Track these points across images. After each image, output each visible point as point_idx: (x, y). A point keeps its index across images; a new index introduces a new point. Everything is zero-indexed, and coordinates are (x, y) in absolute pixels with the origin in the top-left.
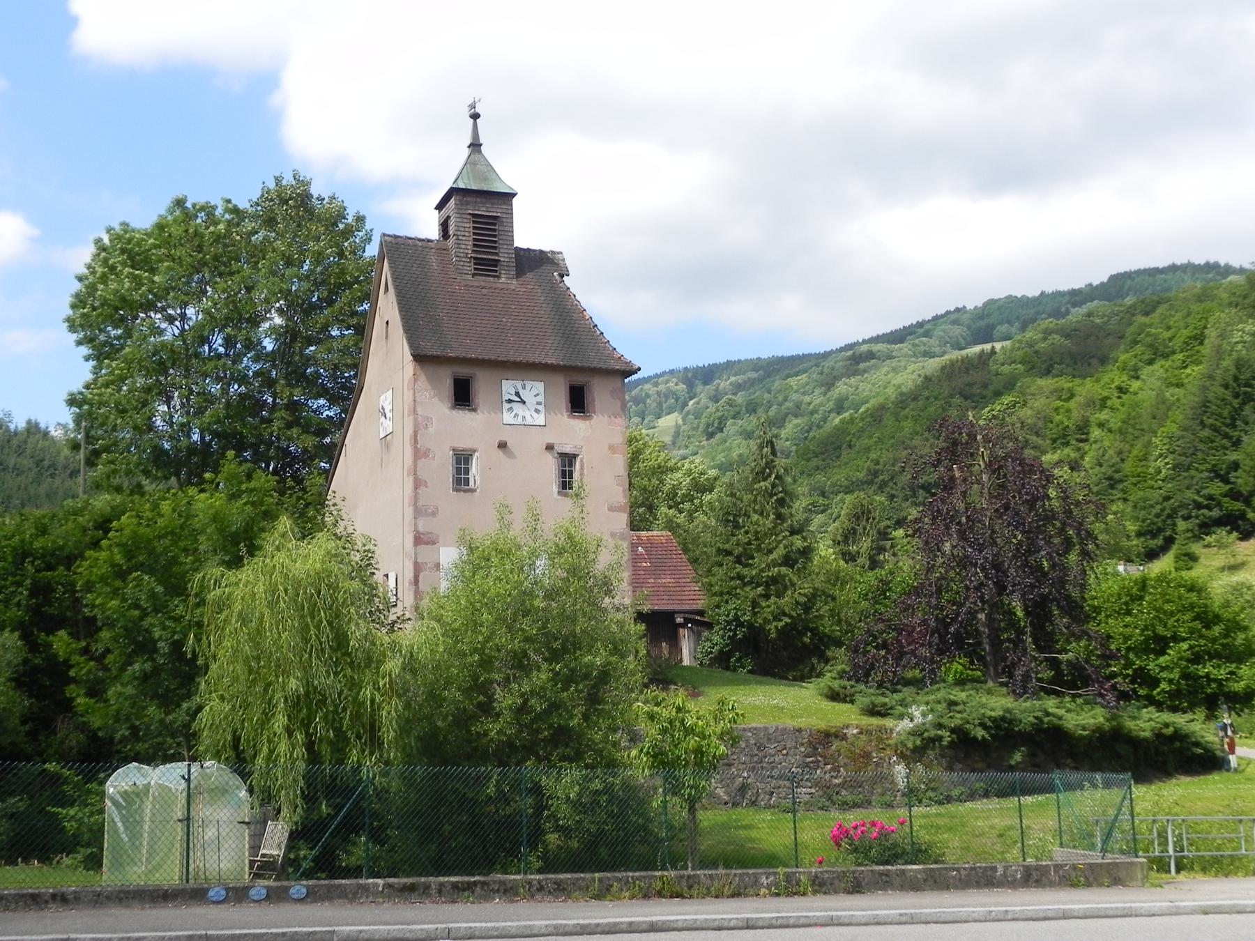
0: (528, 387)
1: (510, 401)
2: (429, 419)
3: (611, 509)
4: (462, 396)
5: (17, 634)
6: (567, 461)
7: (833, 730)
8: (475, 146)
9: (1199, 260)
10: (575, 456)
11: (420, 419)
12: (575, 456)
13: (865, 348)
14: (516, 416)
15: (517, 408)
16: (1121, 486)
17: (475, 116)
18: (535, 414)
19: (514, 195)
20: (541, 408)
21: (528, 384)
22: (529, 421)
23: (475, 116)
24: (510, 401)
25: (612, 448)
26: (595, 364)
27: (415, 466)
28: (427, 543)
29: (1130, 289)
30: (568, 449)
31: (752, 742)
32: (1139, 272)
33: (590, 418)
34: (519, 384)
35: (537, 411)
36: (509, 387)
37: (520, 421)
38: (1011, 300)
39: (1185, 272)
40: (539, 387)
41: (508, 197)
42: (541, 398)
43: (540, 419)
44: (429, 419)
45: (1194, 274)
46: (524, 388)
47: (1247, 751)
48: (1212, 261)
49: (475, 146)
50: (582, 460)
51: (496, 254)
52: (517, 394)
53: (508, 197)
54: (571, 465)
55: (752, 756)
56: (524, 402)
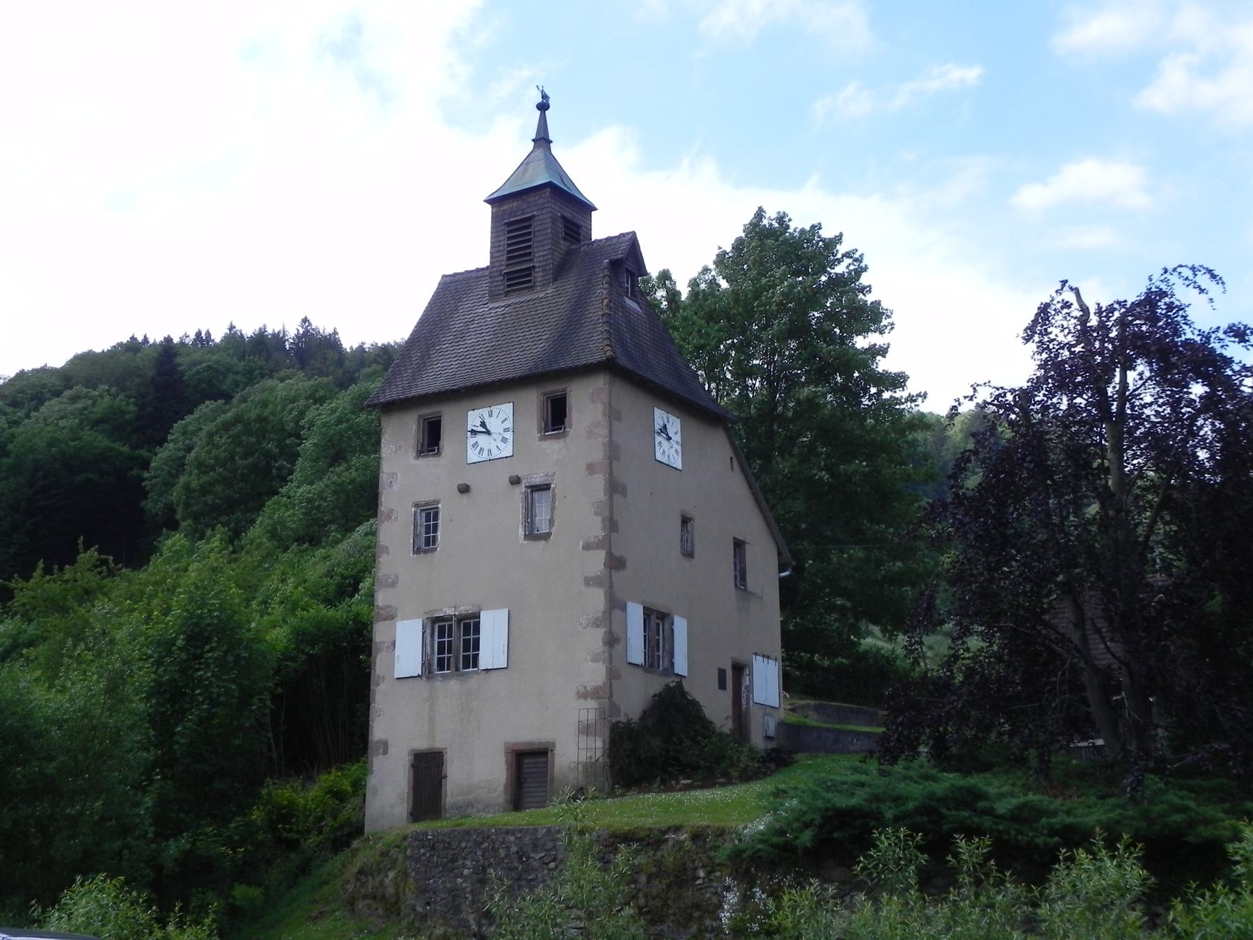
0: (495, 414)
1: (474, 432)
3: (587, 547)
7: (642, 834)
8: (542, 140)
15: (482, 439)
18: (502, 445)
21: (495, 409)
23: (543, 107)
24: (474, 432)
25: (591, 468)
28: (385, 619)
31: (514, 849)
33: (564, 435)
35: (504, 440)
36: (474, 418)
37: (485, 456)
38: (455, 275)
40: (507, 409)
42: (509, 424)
46: (491, 415)
47: (1252, 840)
49: (542, 140)
52: (483, 424)
55: (510, 869)
56: (488, 432)
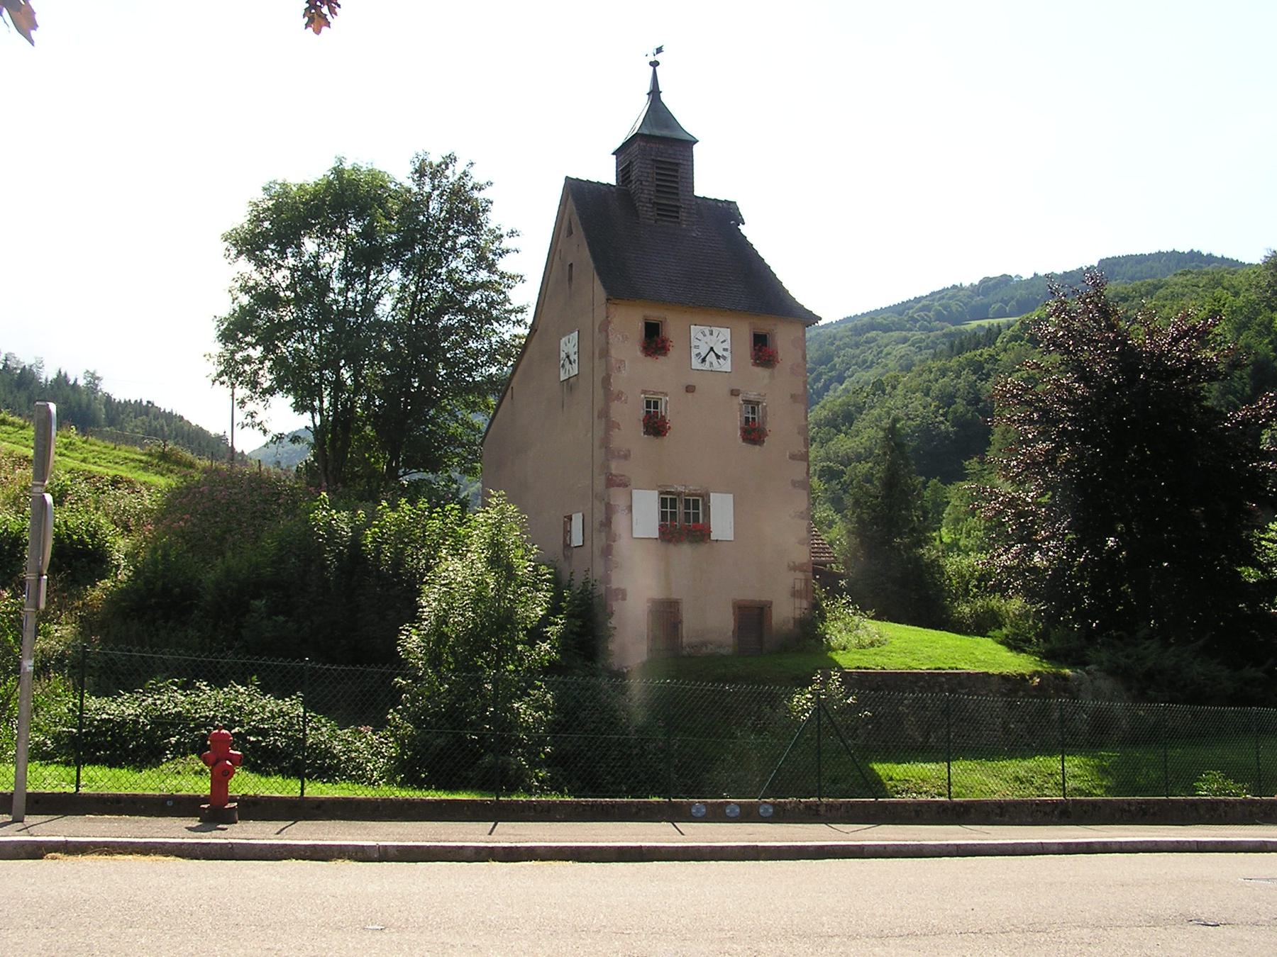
0: (715, 334)
2: (622, 361)
8: (655, 93)
25: (793, 396)
30: (752, 396)
44: (622, 361)
49: (655, 93)
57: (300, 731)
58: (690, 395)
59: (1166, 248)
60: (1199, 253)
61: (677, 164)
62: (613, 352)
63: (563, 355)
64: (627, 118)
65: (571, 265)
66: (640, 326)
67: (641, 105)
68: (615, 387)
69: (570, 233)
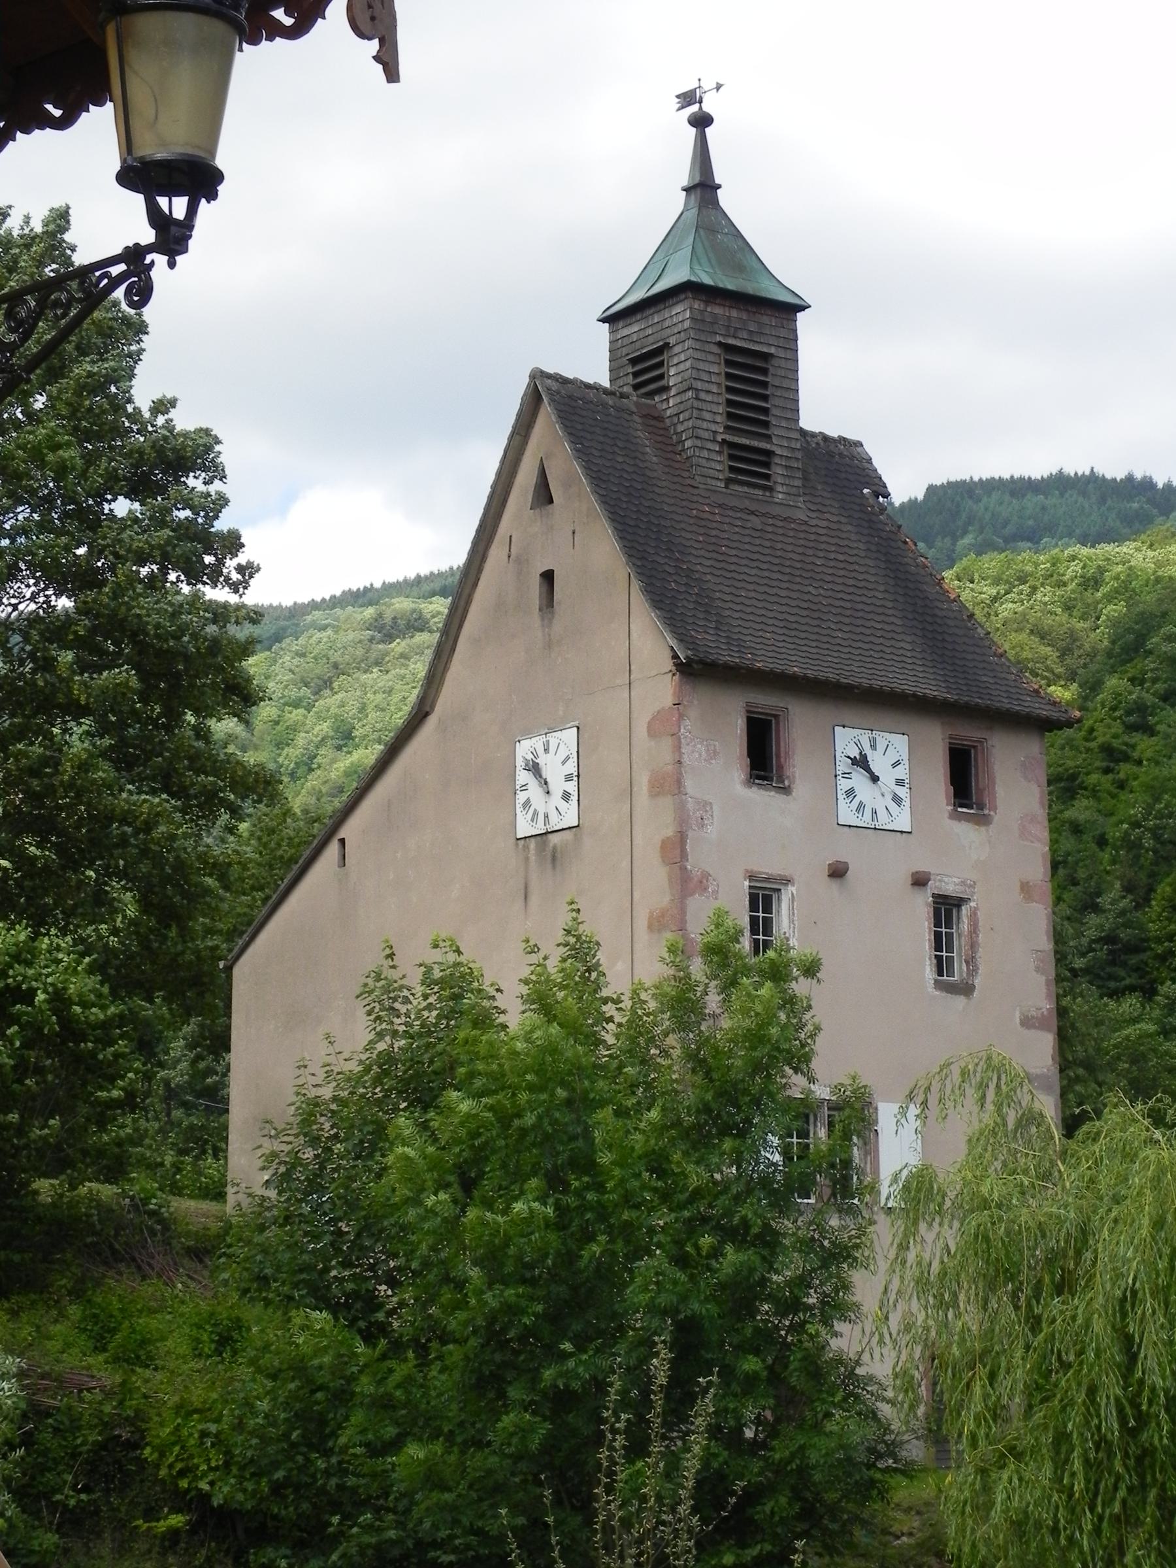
0: (881, 746)
2: (705, 805)
3: (1026, 1022)
4: (763, 759)
5: (839, 1326)
6: (946, 909)
8: (703, 188)
9: (1114, 471)
10: (959, 902)
11: (690, 805)
12: (959, 902)
13: (402, 604)
14: (861, 806)
16: (1133, 960)
17: (702, 122)
18: (893, 806)
19: (803, 308)
20: (903, 792)
21: (882, 738)
22: (883, 821)
23: (702, 122)
25: (1025, 888)
26: (1005, 704)
27: (683, 911)
29: (970, 521)
30: (950, 888)
32: (992, 486)
34: (865, 737)
37: (866, 820)
39: (1084, 494)
41: (790, 309)
42: (902, 772)
43: (902, 820)
44: (705, 805)
45: (1103, 500)
46: (873, 747)
48: (1138, 475)
49: (703, 188)
50: (974, 914)
51: (768, 438)
53: (790, 309)
54: (768, 909)
57: (664, 1523)
58: (834, 884)
59: (1076, 465)
60: (1147, 485)
61: (766, 357)
62: (689, 784)
63: (907, 803)
64: (627, 233)
65: (548, 577)
66: (740, 725)
67: (670, 203)
68: (697, 861)
69: (543, 495)
